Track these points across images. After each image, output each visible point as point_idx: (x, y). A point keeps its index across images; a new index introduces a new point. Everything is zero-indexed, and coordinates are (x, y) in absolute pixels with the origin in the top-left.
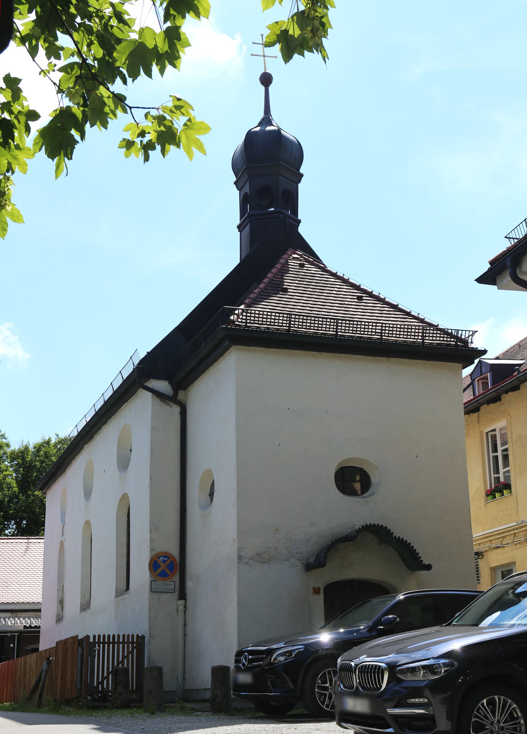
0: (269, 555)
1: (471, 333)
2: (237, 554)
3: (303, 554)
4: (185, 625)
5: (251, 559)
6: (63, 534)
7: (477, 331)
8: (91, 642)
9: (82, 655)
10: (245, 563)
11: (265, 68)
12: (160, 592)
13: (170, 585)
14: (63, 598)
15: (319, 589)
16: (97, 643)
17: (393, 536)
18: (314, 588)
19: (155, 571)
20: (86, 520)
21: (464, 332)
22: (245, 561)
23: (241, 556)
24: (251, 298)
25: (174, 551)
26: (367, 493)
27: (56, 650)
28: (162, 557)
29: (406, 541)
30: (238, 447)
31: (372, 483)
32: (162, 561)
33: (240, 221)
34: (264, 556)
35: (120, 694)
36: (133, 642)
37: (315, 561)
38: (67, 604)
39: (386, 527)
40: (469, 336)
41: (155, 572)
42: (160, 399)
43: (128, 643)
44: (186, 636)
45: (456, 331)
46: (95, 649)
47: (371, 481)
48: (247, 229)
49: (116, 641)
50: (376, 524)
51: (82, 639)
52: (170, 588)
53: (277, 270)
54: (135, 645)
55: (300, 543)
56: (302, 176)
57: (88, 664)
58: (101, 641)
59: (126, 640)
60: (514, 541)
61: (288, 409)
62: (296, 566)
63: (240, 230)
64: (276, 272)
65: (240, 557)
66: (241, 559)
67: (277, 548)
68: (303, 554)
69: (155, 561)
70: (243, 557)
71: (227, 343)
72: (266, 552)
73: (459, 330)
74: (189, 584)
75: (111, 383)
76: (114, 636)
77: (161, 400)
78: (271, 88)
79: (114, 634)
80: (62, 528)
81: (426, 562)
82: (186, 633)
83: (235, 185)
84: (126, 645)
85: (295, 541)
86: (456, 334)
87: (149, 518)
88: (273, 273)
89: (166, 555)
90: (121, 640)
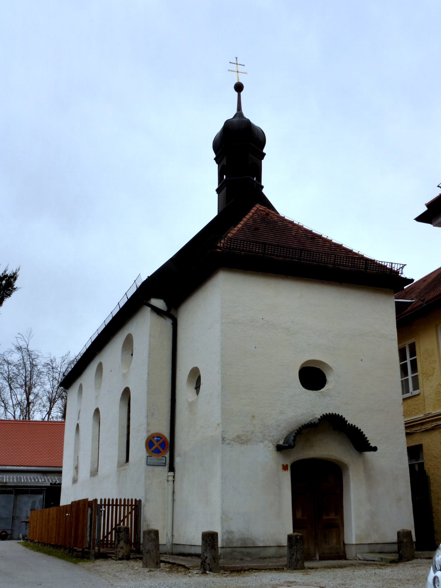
0: (247, 437)
1: (401, 266)
3: (275, 437)
4: (174, 492)
5: (232, 440)
6: (79, 419)
7: (406, 265)
8: (98, 505)
10: (228, 444)
12: (154, 465)
13: (162, 460)
14: (78, 465)
15: (287, 466)
16: (103, 505)
17: (348, 423)
18: (283, 465)
19: (150, 448)
20: (96, 408)
21: (396, 265)
22: (228, 442)
24: (232, 233)
25: (166, 433)
26: (323, 389)
27: (71, 508)
28: (156, 437)
31: (327, 381)
32: (156, 440)
33: (218, 185)
34: (243, 438)
35: (122, 548)
36: (132, 505)
37: (284, 443)
38: (80, 470)
40: (400, 268)
43: (128, 505)
44: (174, 501)
45: (391, 264)
46: (101, 510)
47: (327, 379)
48: (224, 191)
49: (118, 503)
50: (334, 413)
51: (92, 502)
52: (160, 462)
53: (249, 217)
54: (133, 507)
56: (264, 154)
57: (95, 522)
58: (107, 503)
59: (126, 503)
60: (422, 428)
61: (263, 319)
62: (269, 447)
64: (249, 218)
66: (224, 440)
68: (275, 437)
70: (226, 439)
72: (245, 435)
73: (393, 263)
75: (118, 303)
76: (117, 500)
78: (242, 93)
79: (117, 498)
80: (78, 413)
81: (373, 445)
82: (174, 499)
83: (215, 161)
84: (126, 507)
85: (268, 426)
86: (390, 267)
88: (247, 218)
89: (160, 436)
90: (122, 503)
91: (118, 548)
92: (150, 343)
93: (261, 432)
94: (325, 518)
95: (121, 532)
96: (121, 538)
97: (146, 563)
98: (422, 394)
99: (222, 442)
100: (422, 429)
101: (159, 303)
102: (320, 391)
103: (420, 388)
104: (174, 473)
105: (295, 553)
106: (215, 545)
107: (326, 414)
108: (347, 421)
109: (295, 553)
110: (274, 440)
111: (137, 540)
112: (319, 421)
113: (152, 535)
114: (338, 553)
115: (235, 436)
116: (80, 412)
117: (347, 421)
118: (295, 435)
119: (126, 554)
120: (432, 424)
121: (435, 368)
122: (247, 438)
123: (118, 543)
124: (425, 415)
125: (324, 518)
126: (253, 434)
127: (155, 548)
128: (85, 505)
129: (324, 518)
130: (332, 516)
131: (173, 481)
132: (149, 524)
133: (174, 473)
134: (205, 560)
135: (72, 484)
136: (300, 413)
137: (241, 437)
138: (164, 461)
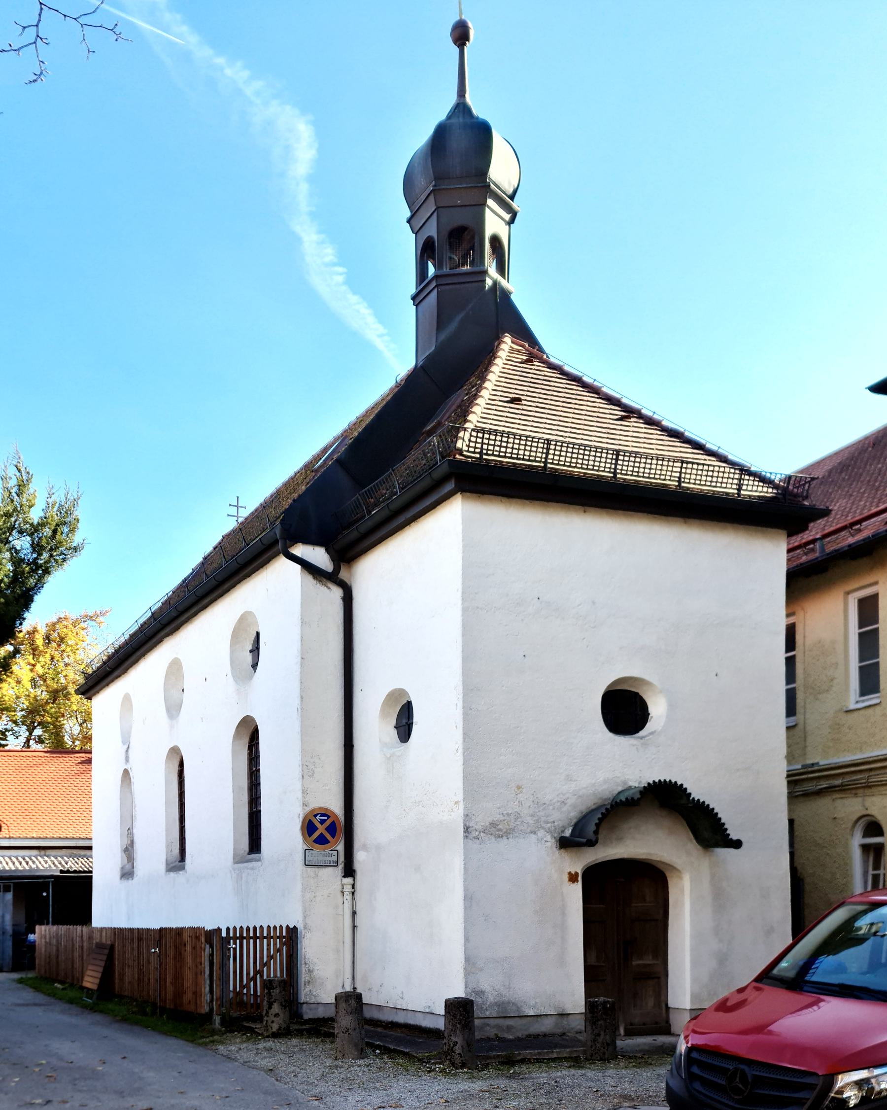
0: (508, 825)
2: (462, 825)
3: (556, 824)
4: (354, 913)
9: (212, 955)
10: (475, 838)
11: (461, 14)
13: (331, 855)
16: (231, 938)
17: (691, 798)
18: (570, 873)
19: (310, 834)
23: (468, 828)
25: (337, 807)
29: (708, 805)
30: (466, 659)
34: (500, 827)
35: (276, 1015)
39: (682, 785)
41: (310, 836)
42: (313, 576)
50: (668, 780)
55: (551, 808)
59: (271, 934)
60: (795, 790)
63: (416, 304)
65: (467, 829)
67: (519, 814)
68: (556, 824)
69: (310, 821)
70: (471, 829)
71: (450, 486)
72: (504, 820)
74: (360, 856)
77: (315, 578)
81: (734, 836)
85: (545, 804)
87: (299, 758)
89: (325, 814)
91: (270, 1015)
92: (302, 637)
93: (532, 816)
94: (635, 962)
95: (274, 989)
96: (274, 998)
97: (342, 1051)
98: (801, 726)
99: (465, 834)
100: (797, 792)
101: (318, 556)
102: (637, 735)
103: (798, 714)
104: (354, 880)
105: (602, 1033)
106: (469, 1022)
107: (654, 781)
108: (690, 794)
109: (602, 1033)
110: (556, 829)
111: (292, 997)
112: (640, 794)
113: (353, 1002)
114: (657, 1023)
115: (488, 824)
116: (128, 748)
117: (690, 794)
118: (597, 821)
119: (284, 1026)
120: (818, 784)
121: (834, 678)
122: (507, 827)
123: (270, 1008)
124: (804, 767)
125: (634, 963)
126: (519, 820)
127: (358, 1024)
128: (197, 938)
129: (634, 963)
130: (648, 960)
131: (351, 894)
132: (311, 969)
133: (354, 880)
134: (452, 1048)
135: (121, 879)
136: (601, 779)
137: (498, 825)
138: (335, 858)
